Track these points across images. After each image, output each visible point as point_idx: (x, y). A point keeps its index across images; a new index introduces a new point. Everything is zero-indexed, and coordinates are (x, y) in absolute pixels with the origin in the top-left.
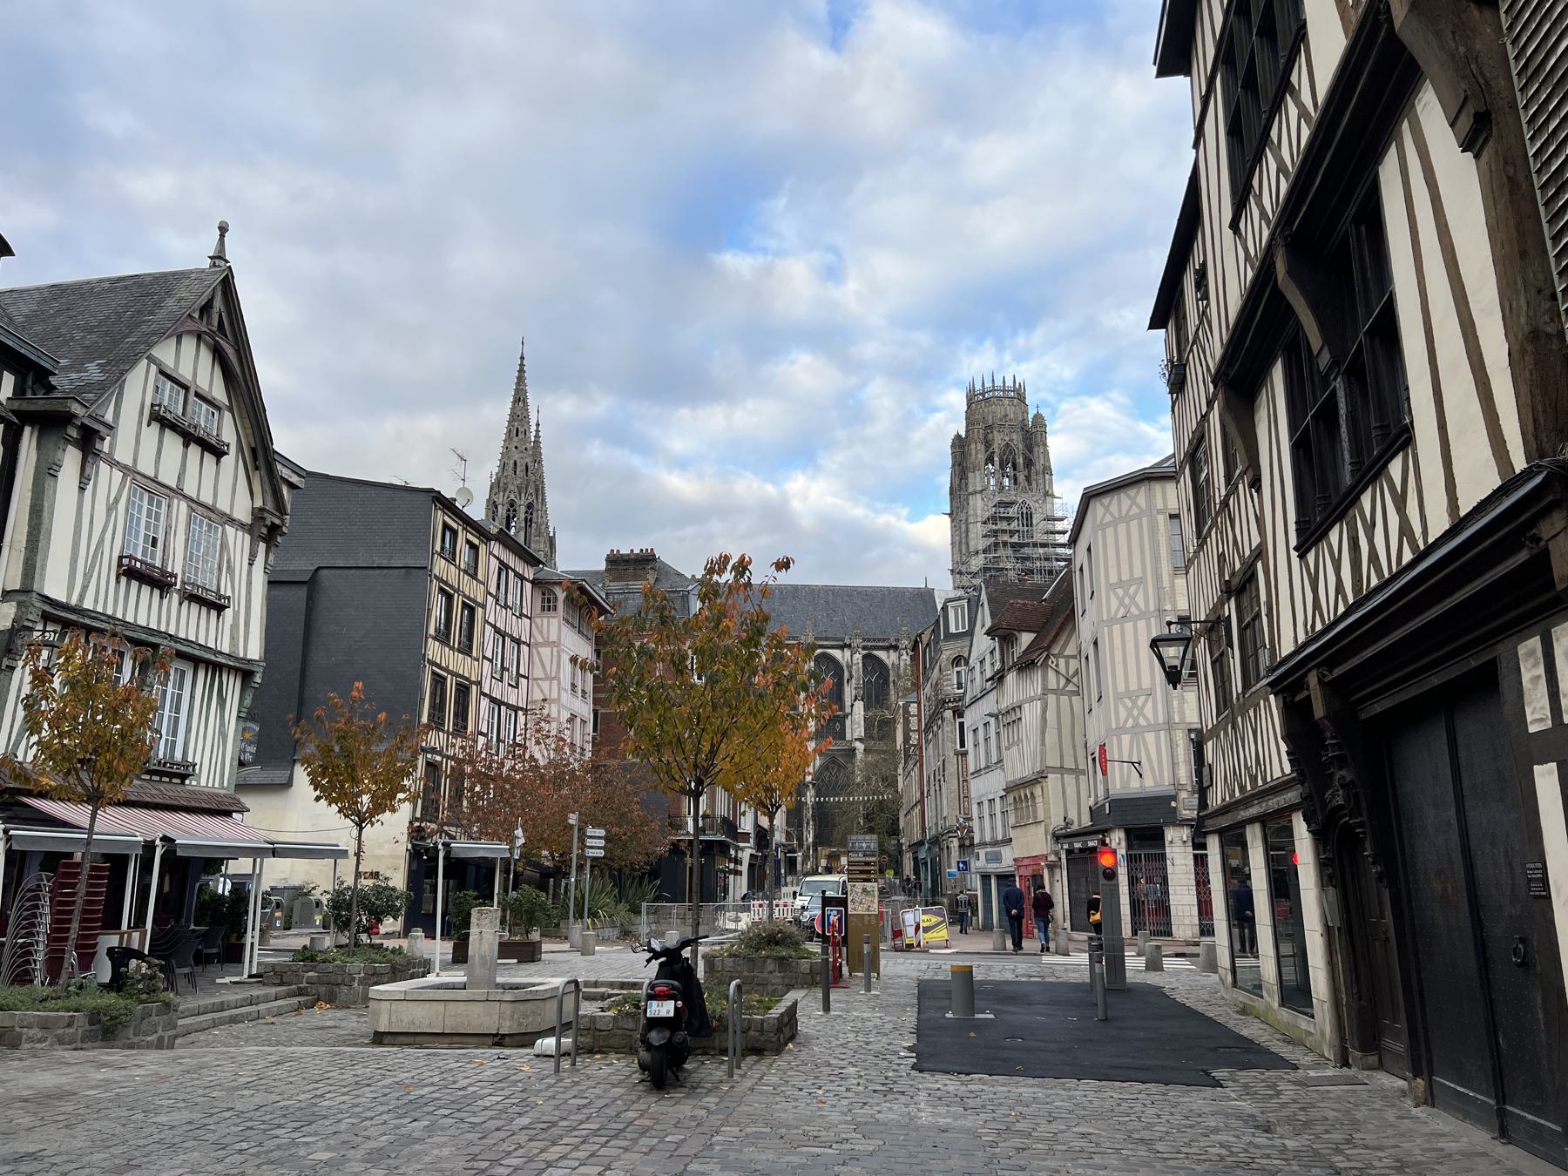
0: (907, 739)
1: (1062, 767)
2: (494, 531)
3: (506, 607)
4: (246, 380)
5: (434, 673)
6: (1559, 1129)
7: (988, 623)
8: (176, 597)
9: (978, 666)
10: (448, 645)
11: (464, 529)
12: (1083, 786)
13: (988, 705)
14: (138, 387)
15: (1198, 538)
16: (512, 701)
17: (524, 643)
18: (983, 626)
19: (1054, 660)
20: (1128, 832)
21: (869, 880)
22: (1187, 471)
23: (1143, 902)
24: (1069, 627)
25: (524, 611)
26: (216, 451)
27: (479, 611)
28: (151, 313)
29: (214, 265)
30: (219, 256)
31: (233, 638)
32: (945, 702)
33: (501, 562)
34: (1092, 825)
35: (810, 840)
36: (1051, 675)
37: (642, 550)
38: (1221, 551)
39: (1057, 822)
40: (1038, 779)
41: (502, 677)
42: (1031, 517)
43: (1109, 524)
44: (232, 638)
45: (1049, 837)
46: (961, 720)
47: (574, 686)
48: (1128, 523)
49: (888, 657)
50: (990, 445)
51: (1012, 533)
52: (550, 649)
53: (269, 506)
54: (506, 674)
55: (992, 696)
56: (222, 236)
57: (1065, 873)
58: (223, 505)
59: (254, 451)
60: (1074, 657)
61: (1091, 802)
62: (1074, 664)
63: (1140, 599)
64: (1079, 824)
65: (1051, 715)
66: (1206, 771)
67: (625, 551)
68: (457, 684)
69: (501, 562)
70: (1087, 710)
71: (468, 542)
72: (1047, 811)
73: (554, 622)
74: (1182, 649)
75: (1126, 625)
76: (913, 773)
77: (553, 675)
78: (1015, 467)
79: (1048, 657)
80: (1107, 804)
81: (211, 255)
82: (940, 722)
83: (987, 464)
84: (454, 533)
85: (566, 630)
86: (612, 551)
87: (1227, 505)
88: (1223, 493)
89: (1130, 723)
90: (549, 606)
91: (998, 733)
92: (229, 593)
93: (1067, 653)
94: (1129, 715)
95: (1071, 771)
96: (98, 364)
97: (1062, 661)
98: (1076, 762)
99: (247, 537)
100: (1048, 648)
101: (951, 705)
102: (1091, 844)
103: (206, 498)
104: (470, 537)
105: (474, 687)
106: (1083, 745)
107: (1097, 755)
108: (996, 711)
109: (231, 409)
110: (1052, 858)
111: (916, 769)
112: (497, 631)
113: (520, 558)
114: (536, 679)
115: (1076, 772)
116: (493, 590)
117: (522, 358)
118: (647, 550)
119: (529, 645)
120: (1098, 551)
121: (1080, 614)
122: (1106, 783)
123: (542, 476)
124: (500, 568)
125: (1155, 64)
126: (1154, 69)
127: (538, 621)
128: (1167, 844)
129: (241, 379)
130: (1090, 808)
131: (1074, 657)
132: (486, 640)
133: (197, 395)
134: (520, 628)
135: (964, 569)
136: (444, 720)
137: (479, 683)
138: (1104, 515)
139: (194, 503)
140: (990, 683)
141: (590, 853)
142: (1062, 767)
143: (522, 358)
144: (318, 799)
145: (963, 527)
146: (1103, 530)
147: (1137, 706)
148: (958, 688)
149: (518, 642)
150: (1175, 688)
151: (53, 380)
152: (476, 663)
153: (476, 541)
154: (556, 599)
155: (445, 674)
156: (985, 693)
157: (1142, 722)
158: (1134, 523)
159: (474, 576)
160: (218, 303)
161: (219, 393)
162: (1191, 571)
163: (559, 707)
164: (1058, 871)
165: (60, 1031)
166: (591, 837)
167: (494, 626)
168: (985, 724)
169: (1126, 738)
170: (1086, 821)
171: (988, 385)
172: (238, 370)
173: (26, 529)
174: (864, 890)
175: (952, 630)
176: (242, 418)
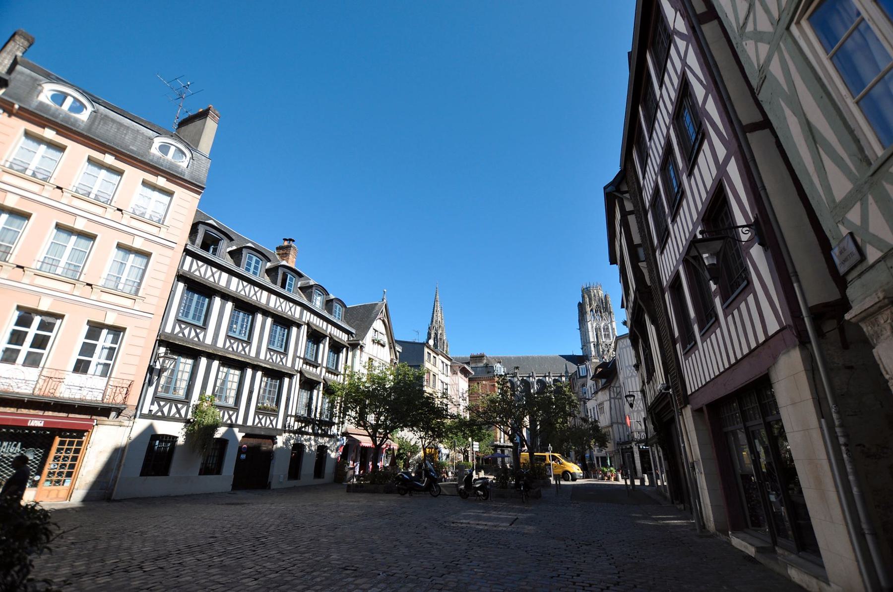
6: (535, 454)
14: (370, 334)
26: (383, 346)
27: (437, 376)
35: (539, 444)
39: (617, 439)
61: (628, 433)
67: (475, 354)
78: (601, 312)
93: (616, 386)
95: (620, 423)
97: (615, 389)
112: (442, 382)
169: (635, 414)
175: (581, 375)
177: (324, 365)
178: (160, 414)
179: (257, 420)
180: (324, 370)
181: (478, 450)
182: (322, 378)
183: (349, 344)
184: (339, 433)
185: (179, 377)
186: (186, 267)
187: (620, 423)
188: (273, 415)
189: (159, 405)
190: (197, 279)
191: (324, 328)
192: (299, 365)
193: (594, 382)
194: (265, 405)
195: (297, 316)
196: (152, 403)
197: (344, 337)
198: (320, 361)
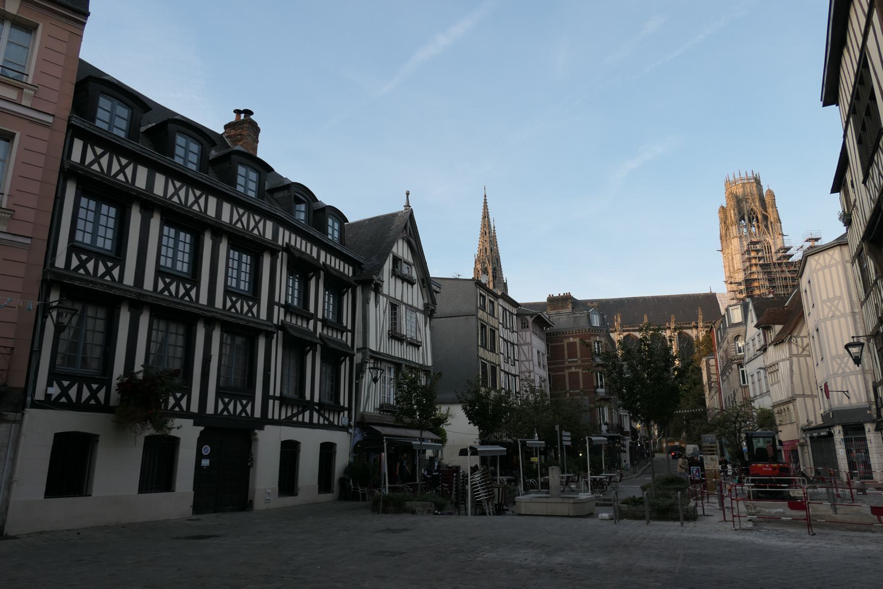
0: (709, 378)
1: (804, 394)
2: (500, 293)
3: (507, 328)
4: (419, 253)
5: (482, 362)
7: (755, 322)
8: (405, 344)
9: (751, 343)
10: (486, 349)
11: (488, 295)
12: (817, 404)
13: (759, 362)
15: (865, 293)
16: (513, 372)
17: (516, 344)
18: (752, 321)
19: (795, 339)
20: (844, 427)
21: (713, 454)
22: (857, 261)
23: (855, 462)
24: (801, 322)
25: (514, 330)
26: (411, 283)
28: (388, 233)
29: (406, 209)
30: (408, 205)
31: (423, 358)
32: (732, 360)
33: (503, 308)
34: (824, 424)
36: (794, 347)
37: (564, 294)
38: (876, 303)
39: (803, 422)
40: (792, 400)
41: (508, 362)
42: (771, 248)
43: (819, 269)
44: (423, 358)
45: (799, 430)
46: (742, 369)
47: (539, 364)
48: (830, 268)
49: (692, 333)
50: (742, 210)
51: (760, 259)
52: (527, 347)
53: (430, 302)
54: (509, 360)
55: (761, 358)
56: (408, 197)
57: (810, 449)
58: (415, 305)
59: (423, 280)
60: (806, 337)
61: (822, 411)
62: (806, 341)
63: (840, 307)
64: (816, 423)
65: (795, 368)
66: (879, 400)
67: (556, 295)
68: (491, 366)
69: (503, 308)
70: (815, 364)
71: (490, 300)
72: (797, 416)
73: (528, 333)
74: (861, 348)
75: (834, 321)
76: (715, 397)
77: (530, 359)
78: (757, 221)
79: (791, 338)
80: (831, 413)
81: (405, 205)
82: (730, 370)
83: (741, 221)
84: (484, 297)
85: (534, 337)
86: (550, 295)
87: (877, 283)
88: (875, 278)
89: (840, 371)
90: (525, 326)
91: (766, 377)
92: (420, 341)
94: (840, 367)
95: (809, 396)
96: (376, 257)
97: (799, 340)
98: (811, 391)
99: (423, 315)
100: (791, 333)
101: (735, 361)
102: (822, 434)
103: (410, 303)
104: (491, 298)
105: (498, 367)
106: (815, 382)
107: (823, 388)
108: (764, 367)
109: (414, 266)
110: (802, 441)
111: (717, 395)
112: (504, 340)
113: (511, 304)
114: (522, 361)
115: (812, 396)
116: (501, 322)
117: (485, 196)
118: (567, 293)
119: (517, 345)
120: (814, 282)
121: (807, 315)
122: (829, 402)
123: (498, 254)
124: (503, 311)
125: (821, 100)
126: (821, 103)
127: (521, 333)
128: (866, 432)
129: (417, 253)
130: (821, 414)
131: (806, 337)
132: (501, 346)
133: (405, 262)
134: (513, 337)
135: (733, 280)
136: (487, 383)
137: (499, 365)
138: (816, 265)
139: (407, 305)
140: (759, 352)
141: (565, 443)
142: (804, 394)
143: (485, 196)
144: (470, 423)
145: (730, 257)
146: (816, 272)
147: (843, 369)
148: (739, 352)
149: (513, 344)
150: (858, 366)
151: (363, 266)
152: (498, 356)
153: (493, 300)
154: (528, 322)
155: (486, 362)
156: (756, 357)
157: (847, 370)
158: (834, 269)
159: (493, 316)
160: (409, 224)
161: (410, 260)
162: (863, 307)
163: (534, 374)
164: (806, 447)
165: (428, 509)
166: (565, 436)
167: (503, 338)
168: (758, 372)
170: (820, 421)
171: (737, 177)
172: (416, 249)
173: (361, 325)
174: (712, 459)
176: (418, 267)
177: (320, 316)
178: (63, 400)
179: (221, 406)
180: (319, 324)
181: (569, 443)
182: (318, 335)
183: (355, 281)
184: (352, 423)
185: (89, 340)
186: (76, 157)
187: (809, 396)
188: (245, 397)
189: (61, 386)
190: (98, 176)
191: (315, 255)
192: (279, 316)
193: (761, 331)
194: (434, 491)
195: (269, 235)
196: (50, 384)
197: (348, 271)
198: (312, 310)
